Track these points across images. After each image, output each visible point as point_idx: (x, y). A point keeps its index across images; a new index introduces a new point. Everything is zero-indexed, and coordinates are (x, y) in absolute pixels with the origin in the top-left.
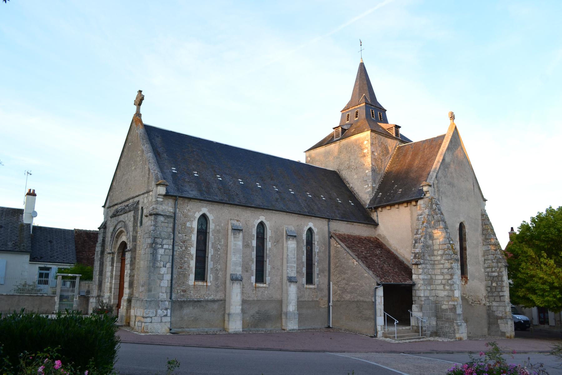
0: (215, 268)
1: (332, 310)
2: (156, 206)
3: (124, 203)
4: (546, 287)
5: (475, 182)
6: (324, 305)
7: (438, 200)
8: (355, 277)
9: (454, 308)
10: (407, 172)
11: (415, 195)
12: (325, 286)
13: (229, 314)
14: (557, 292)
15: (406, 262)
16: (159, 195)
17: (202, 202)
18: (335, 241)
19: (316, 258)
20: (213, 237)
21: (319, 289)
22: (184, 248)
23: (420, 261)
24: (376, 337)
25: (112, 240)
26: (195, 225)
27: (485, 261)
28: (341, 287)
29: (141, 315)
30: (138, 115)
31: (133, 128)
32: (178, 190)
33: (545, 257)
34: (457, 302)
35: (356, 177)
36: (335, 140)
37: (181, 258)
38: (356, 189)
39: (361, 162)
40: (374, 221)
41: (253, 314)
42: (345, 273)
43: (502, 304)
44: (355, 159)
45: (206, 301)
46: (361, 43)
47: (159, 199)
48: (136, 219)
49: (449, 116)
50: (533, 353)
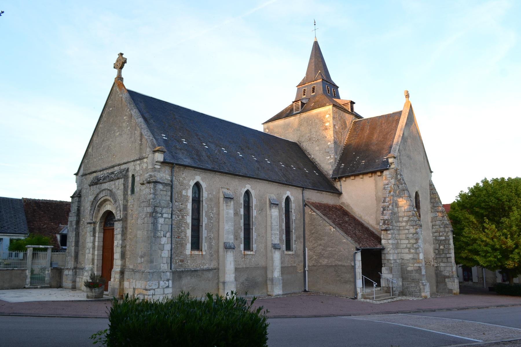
0: (209, 237)
1: (308, 274)
2: (154, 173)
3: (106, 171)
4: (489, 249)
5: (424, 155)
6: (300, 270)
7: (401, 170)
8: (333, 243)
9: (419, 269)
10: (367, 145)
11: (380, 166)
12: (301, 252)
13: (224, 283)
14: (497, 253)
15: (371, 228)
16: (156, 162)
17: (196, 170)
18: (310, 209)
19: (293, 226)
20: (206, 205)
21: (296, 255)
22: (180, 217)
23: (389, 228)
24: (356, 298)
25: (93, 209)
26: (190, 193)
27: (433, 226)
28: (318, 253)
29: (143, 287)
30: (119, 79)
31: (114, 92)
32: (173, 157)
33: (487, 223)
34: (422, 264)
35: (317, 148)
36: (294, 113)
37: (179, 227)
38: (317, 160)
40: (337, 190)
41: (242, 282)
42: (321, 240)
43: (449, 264)
44: (316, 132)
45: (201, 270)
46: (315, 23)
47: (156, 166)
48: (126, 187)
49: (405, 94)
50: (492, 307)
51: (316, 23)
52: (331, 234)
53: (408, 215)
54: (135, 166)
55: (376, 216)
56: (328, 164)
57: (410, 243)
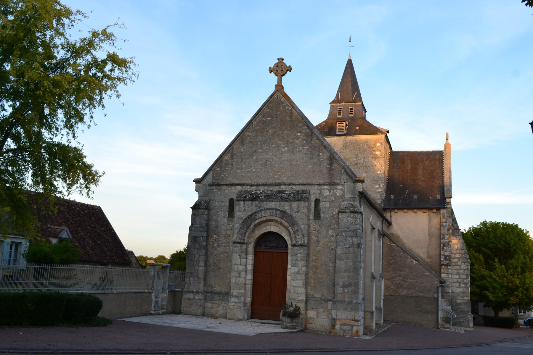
39: (372, 162)
51: (351, 40)
52: (413, 266)
53: (461, 253)
54: (320, 190)
55: (428, 250)
56: (377, 193)
57: (461, 278)
